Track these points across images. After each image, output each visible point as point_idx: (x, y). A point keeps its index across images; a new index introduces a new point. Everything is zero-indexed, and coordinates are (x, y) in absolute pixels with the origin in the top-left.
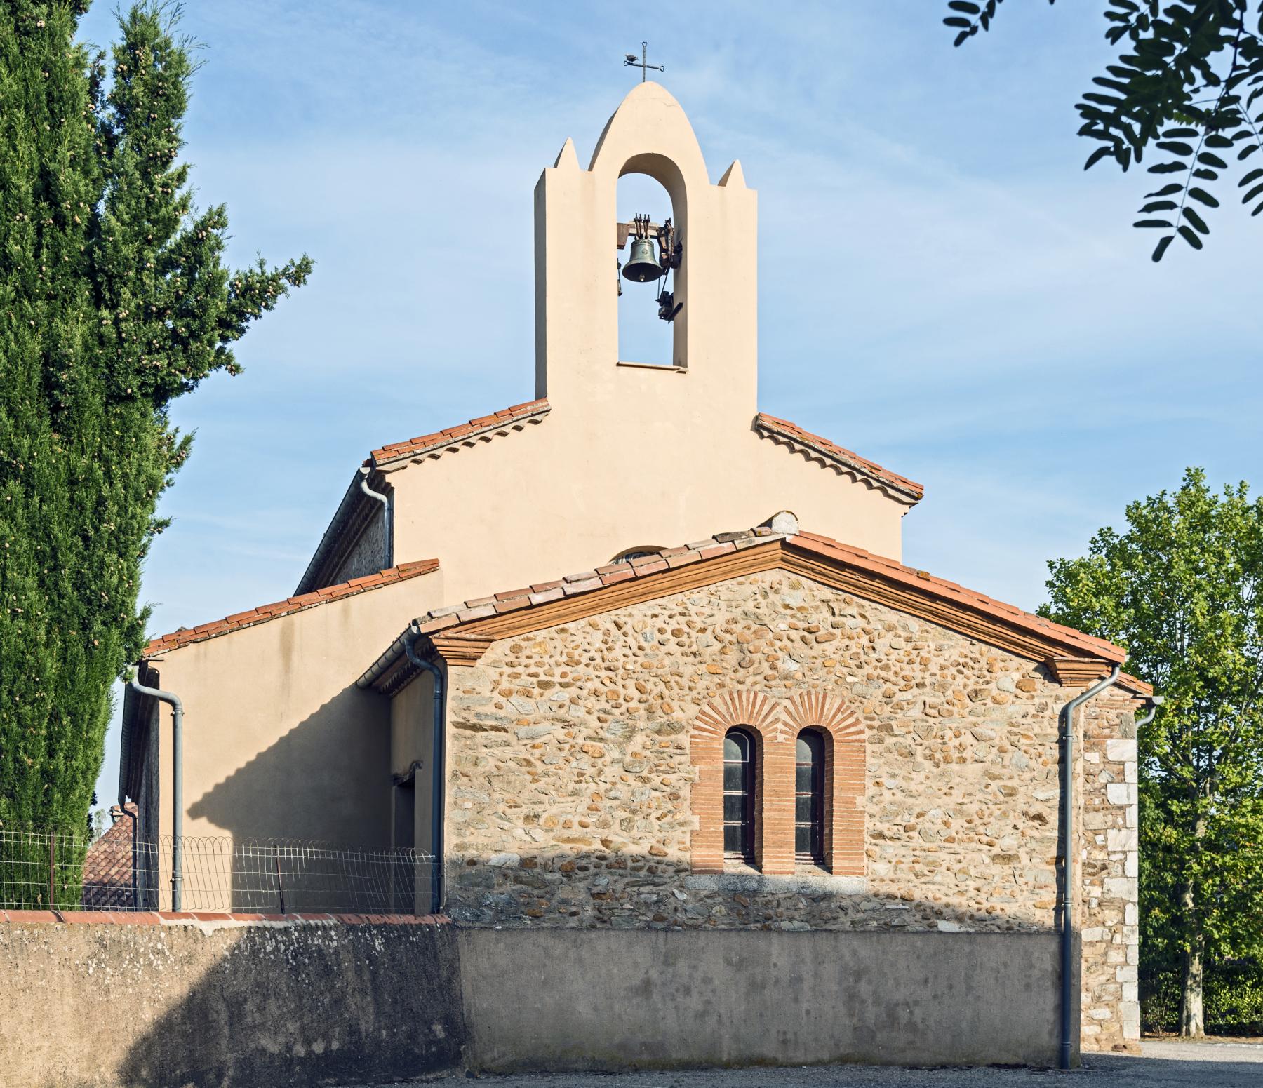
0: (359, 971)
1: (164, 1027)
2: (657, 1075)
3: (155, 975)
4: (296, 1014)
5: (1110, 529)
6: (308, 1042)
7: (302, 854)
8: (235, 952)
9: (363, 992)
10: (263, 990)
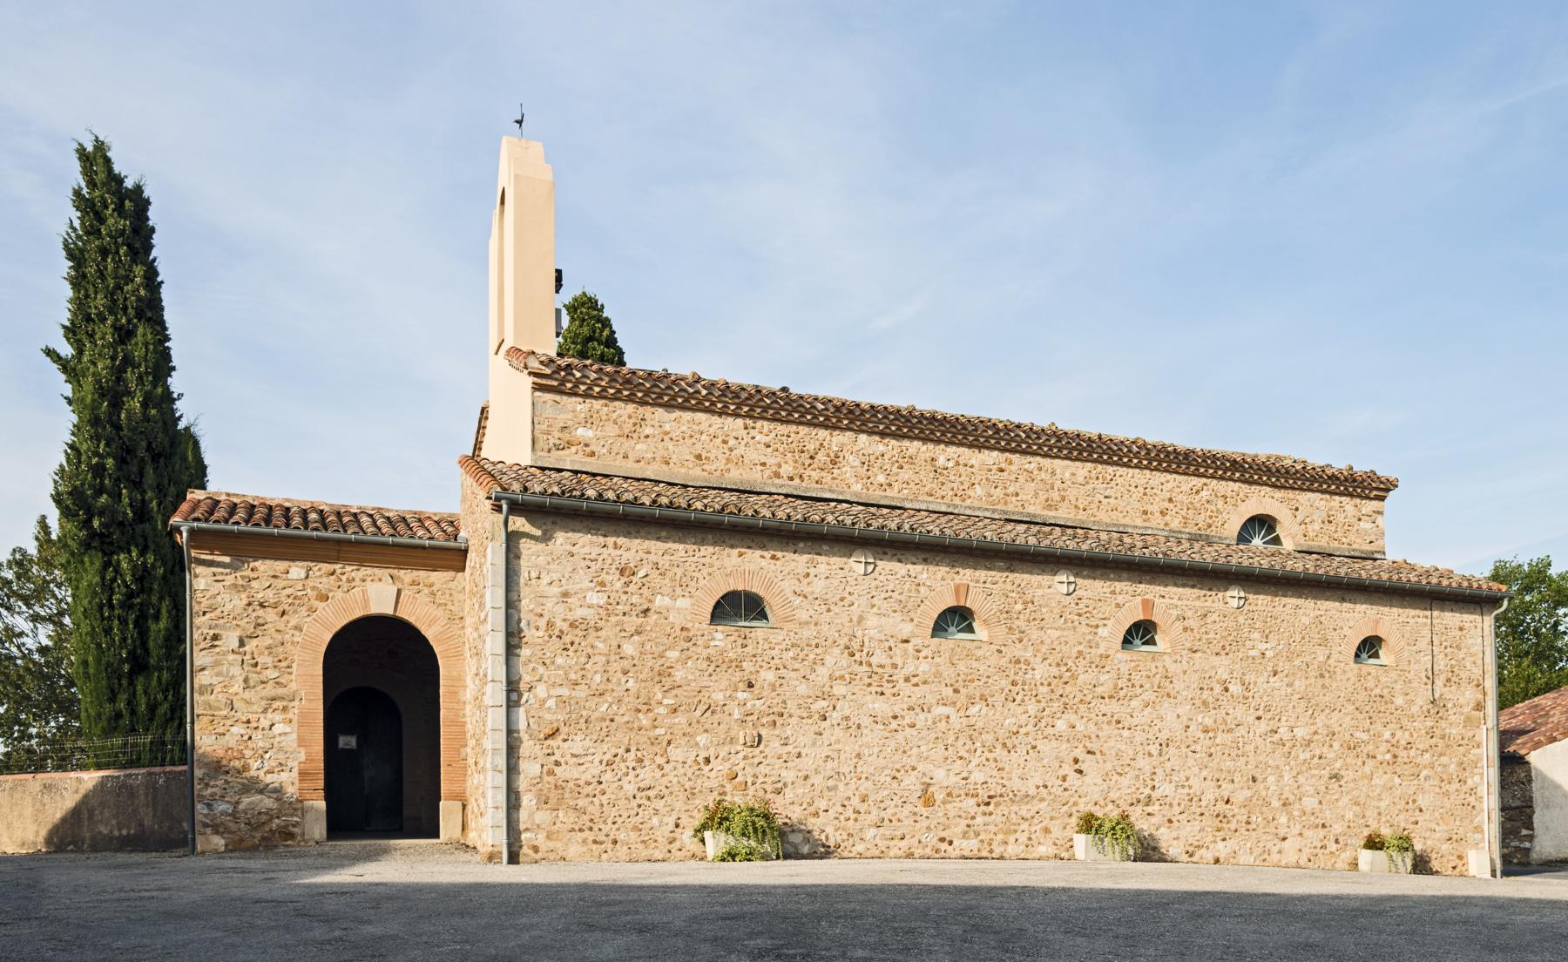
0: (146, 795)
1: (64, 820)
2: (877, 438)
3: (63, 797)
4: (116, 816)
5: (784, 389)
6: (120, 830)
7: (1526, 568)
8: (95, 787)
9: (147, 806)
10: (103, 805)
